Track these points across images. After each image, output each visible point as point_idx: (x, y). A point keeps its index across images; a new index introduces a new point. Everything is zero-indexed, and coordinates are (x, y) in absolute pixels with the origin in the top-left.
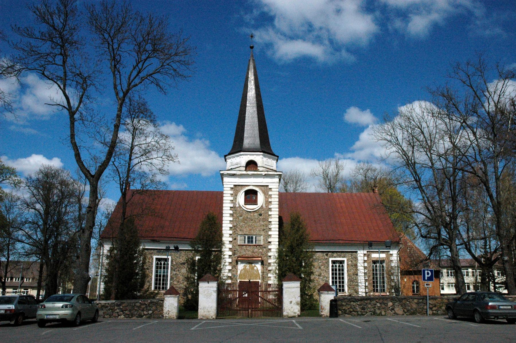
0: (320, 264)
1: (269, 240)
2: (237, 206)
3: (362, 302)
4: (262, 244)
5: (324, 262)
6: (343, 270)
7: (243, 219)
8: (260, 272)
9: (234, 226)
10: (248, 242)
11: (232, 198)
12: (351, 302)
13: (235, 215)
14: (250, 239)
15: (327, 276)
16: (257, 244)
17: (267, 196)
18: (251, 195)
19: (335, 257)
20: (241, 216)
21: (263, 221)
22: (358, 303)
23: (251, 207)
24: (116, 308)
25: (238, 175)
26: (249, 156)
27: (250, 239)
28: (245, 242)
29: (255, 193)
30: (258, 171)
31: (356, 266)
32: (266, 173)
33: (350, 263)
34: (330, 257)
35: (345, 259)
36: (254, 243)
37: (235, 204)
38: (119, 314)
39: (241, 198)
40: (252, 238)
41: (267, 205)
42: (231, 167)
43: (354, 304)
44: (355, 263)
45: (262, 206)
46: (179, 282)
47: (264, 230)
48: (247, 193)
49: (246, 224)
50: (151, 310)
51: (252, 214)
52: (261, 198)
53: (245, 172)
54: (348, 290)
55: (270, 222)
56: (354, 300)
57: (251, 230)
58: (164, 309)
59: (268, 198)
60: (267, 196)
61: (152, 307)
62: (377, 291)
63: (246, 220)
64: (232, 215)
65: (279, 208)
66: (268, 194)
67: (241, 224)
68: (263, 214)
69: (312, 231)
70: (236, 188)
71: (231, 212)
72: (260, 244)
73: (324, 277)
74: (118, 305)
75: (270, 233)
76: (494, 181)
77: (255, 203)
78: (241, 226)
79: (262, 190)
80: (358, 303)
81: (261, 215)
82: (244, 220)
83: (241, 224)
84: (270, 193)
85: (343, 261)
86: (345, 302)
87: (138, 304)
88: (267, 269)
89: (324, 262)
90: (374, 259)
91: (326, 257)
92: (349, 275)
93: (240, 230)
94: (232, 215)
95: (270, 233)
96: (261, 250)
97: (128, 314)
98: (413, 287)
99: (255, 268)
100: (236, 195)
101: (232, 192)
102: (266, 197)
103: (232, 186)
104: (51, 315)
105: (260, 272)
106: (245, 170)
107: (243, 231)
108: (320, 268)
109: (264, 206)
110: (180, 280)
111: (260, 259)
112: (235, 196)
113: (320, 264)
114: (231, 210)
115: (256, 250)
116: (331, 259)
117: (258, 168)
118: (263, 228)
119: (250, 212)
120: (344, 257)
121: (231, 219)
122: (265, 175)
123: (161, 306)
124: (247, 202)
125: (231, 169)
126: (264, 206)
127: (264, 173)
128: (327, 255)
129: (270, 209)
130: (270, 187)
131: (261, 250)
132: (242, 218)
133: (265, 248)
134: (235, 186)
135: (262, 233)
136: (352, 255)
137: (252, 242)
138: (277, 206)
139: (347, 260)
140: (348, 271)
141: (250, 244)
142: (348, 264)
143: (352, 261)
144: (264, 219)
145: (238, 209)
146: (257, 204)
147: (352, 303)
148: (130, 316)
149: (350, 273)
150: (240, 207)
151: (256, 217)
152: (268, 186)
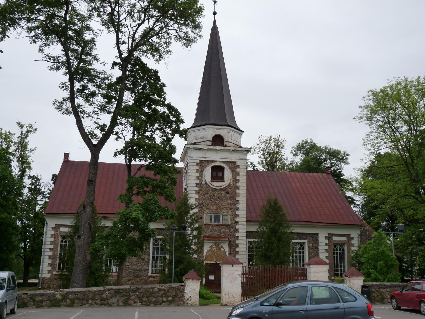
1: (237, 220)
2: (203, 182)
3: (392, 289)
4: (229, 224)
6: (303, 253)
7: (210, 196)
8: (227, 253)
9: (200, 204)
10: (215, 221)
11: (198, 174)
12: (380, 288)
13: (201, 192)
14: (217, 218)
16: (224, 223)
17: (235, 174)
18: (218, 172)
20: (207, 194)
21: (231, 200)
22: (388, 290)
23: (217, 184)
24: (131, 294)
25: (205, 149)
26: (215, 130)
27: (217, 218)
28: (211, 221)
29: (222, 169)
30: (225, 146)
31: (317, 248)
32: (234, 148)
33: (311, 245)
35: (306, 241)
36: (221, 223)
37: (201, 180)
38: (136, 301)
39: (207, 174)
40: (219, 216)
41: (234, 182)
42: (195, 141)
43: (384, 291)
44: (316, 245)
45: (229, 184)
46: (132, 263)
47: (231, 209)
48: (214, 169)
49: (212, 202)
50: (170, 296)
51: (219, 192)
52: (228, 174)
53: (212, 147)
55: (238, 200)
56: (383, 286)
57: (217, 208)
58: (185, 295)
59: (236, 176)
60: (235, 174)
61: (172, 293)
62: (338, 275)
63: (212, 198)
64: (197, 193)
65: (247, 186)
66: (235, 171)
67: (208, 202)
68: (231, 192)
69: (289, 212)
70: (202, 164)
71: (197, 189)
72: (226, 223)
74: (133, 291)
75: (238, 212)
76: (320, 174)
77: (222, 179)
78: (208, 205)
79: (229, 167)
80: (388, 290)
81: (228, 193)
82: (210, 198)
83: (208, 202)
84: (238, 170)
86: (374, 288)
87: (156, 290)
88: (234, 251)
90: (335, 243)
93: (207, 209)
94: (197, 193)
95: (238, 212)
96: (228, 231)
97: (146, 302)
98: (335, 269)
99: (222, 249)
100: (202, 171)
101: (198, 168)
102: (233, 175)
103: (198, 162)
105: (227, 253)
106: (211, 145)
107: (209, 210)
109: (232, 184)
110: (133, 261)
111: (227, 239)
112: (201, 171)
114: (196, 186)
115: (223, 230)
117: (226, 143)
118: (230, 206)
119: (217, 189)
121: (197, 196)
122: (233, 151)
123: (181, 292)
124: (214, 178)
125: (195, 143)
126: (232, 184)
127: (232, 149)
129: (238, 188)
130: (237, 164)
131: (228, 231)
132: (208, 195)
133: (232, 228)
134: (201, 161)
135: (230, 212)
136: (313, 237)
137: (219, 221)
138: (245, 184)
139: (308, 242)
140: (309, 254)
141: (217, 224)
142: (308, 247)
143: (312, 244)
144: (231, 197)
145: (205, 186)
146: (224, 181)
147: (381, 290)
148: (148, 303)
149: (310, 255)
150: (206, 183)
151: (223, 195)
152: (236, 162)
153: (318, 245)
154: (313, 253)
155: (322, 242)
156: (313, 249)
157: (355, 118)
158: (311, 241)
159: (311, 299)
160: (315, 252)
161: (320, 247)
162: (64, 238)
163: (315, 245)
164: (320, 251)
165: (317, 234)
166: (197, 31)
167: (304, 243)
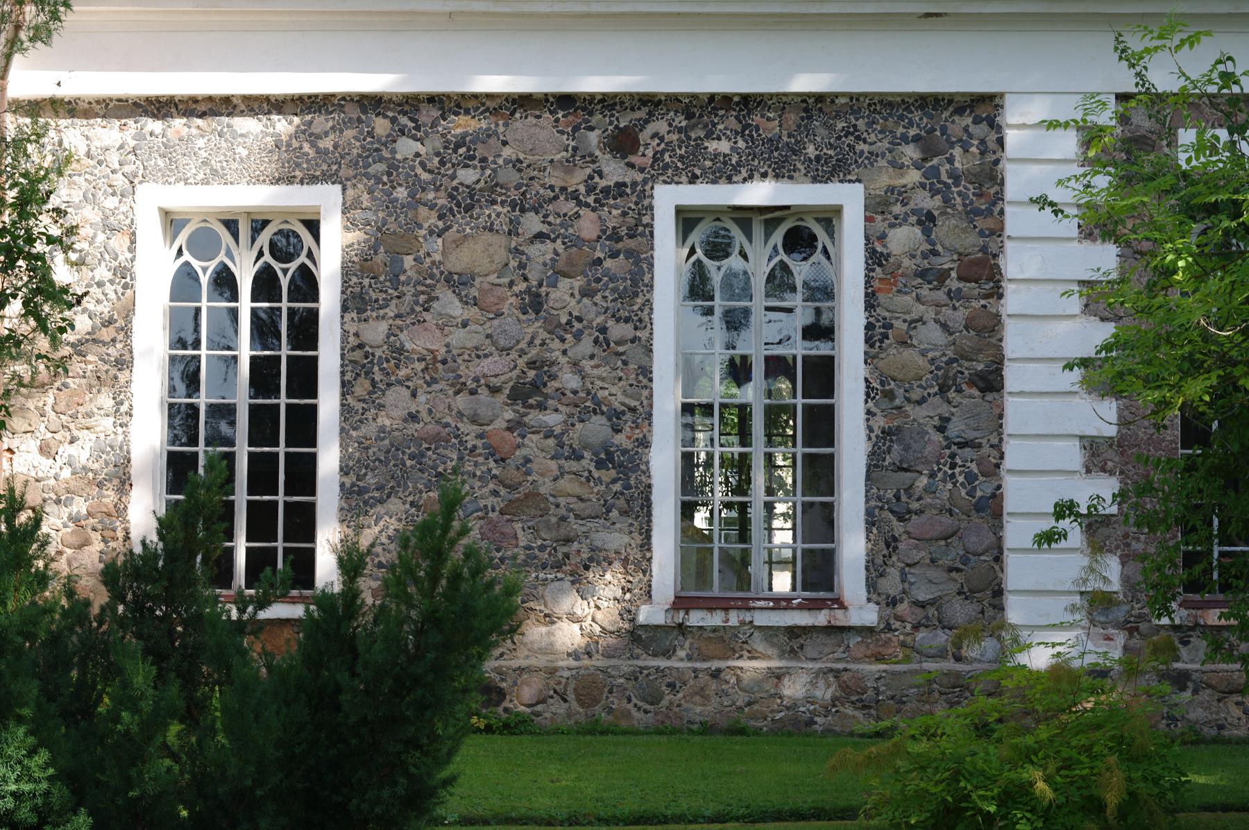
0: (541, 253)
5: (588, 226)
15: (616, 395)
19: (724, 172)
31: (984, 273)
33: (904, 238)
34: (662, 170)
35: (848, 197)
54: (875, 570)
64: (1097, 299)
73: (587, 405)
85: (830, 217)
89: (588, 226)
91: (614, 171)
92: (878, 392)
104: (184, 12)
108: (534, 303)
113: (541, 253)
116: (667, 199)
120: (831, 169)
128: (624, 143)
136: (929, 148)
139: (876, 207)
142: (875, 258)
143: (927, 220)
149: (894, 356)
153: (997, 231)
154: (931, 334)
155: (1040, 154)
156: (932, 276)
157: (59, 84)
158: (902, 195)
159: (812, 605)
160: (958, 317)
161: (1017, 262)
162: (202, 244)
163: (951, 233)
164: (1014, 301)
165: (985, 107)
166: (989, 397)
167: (830, 217)
